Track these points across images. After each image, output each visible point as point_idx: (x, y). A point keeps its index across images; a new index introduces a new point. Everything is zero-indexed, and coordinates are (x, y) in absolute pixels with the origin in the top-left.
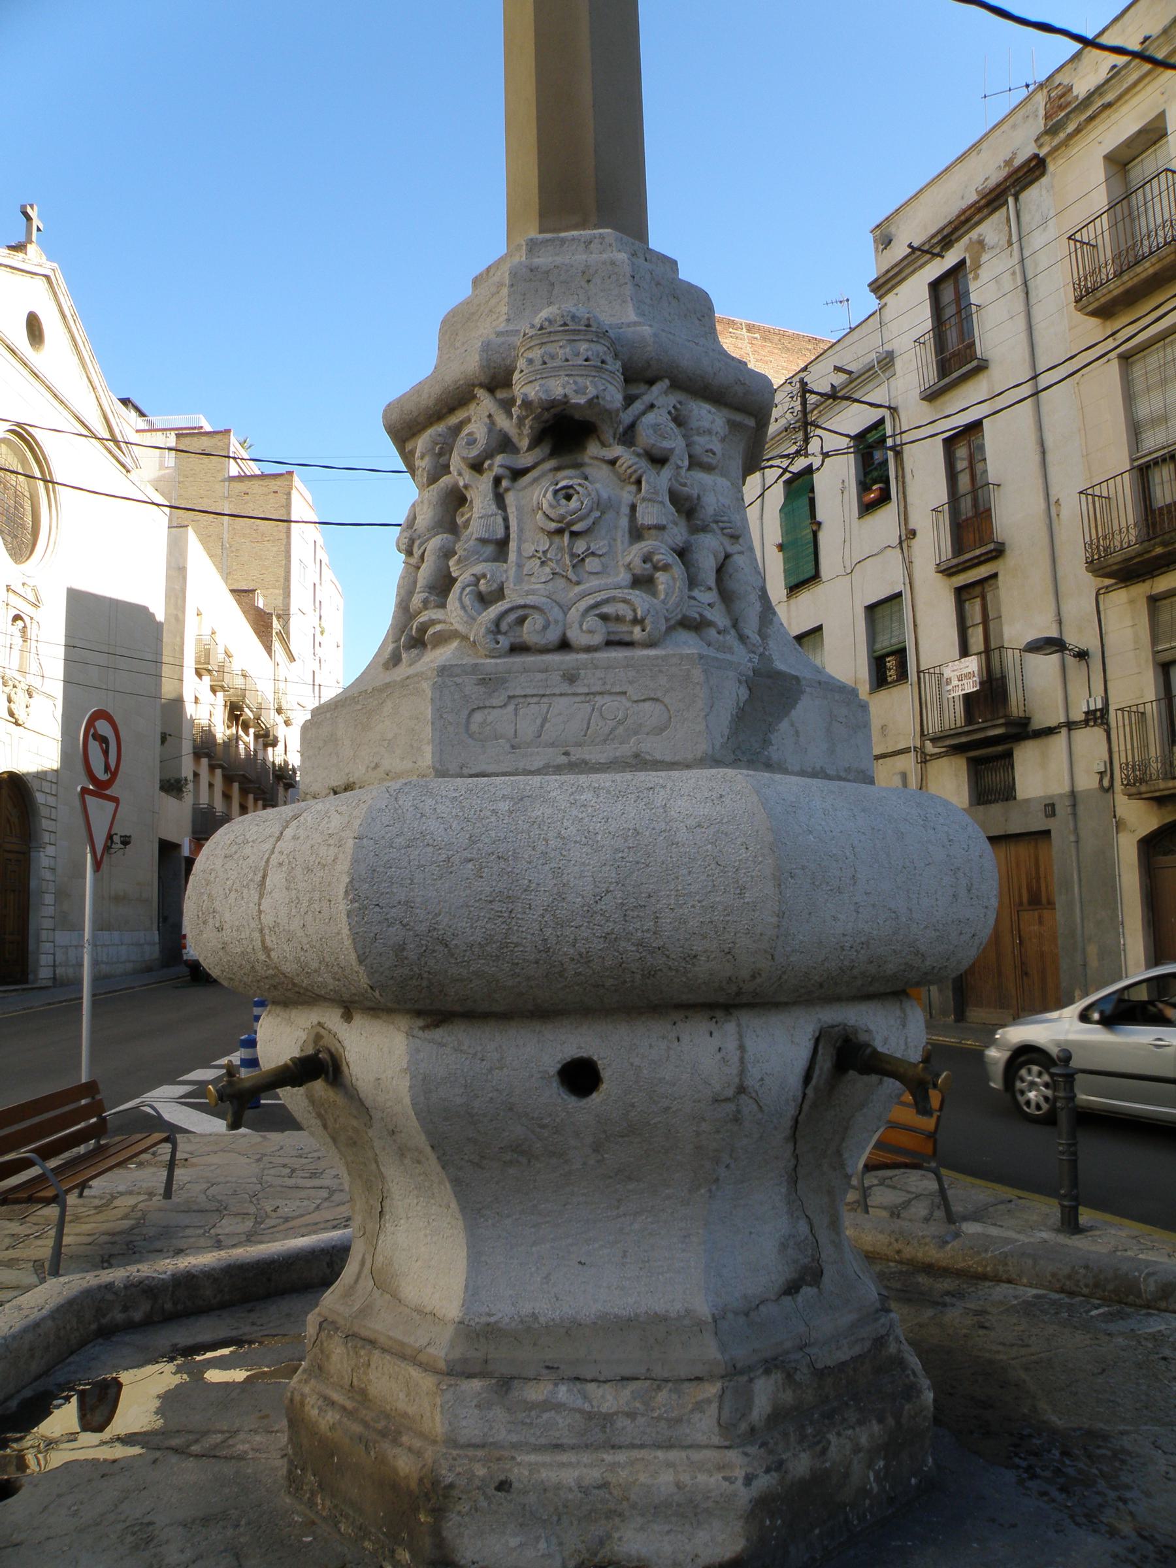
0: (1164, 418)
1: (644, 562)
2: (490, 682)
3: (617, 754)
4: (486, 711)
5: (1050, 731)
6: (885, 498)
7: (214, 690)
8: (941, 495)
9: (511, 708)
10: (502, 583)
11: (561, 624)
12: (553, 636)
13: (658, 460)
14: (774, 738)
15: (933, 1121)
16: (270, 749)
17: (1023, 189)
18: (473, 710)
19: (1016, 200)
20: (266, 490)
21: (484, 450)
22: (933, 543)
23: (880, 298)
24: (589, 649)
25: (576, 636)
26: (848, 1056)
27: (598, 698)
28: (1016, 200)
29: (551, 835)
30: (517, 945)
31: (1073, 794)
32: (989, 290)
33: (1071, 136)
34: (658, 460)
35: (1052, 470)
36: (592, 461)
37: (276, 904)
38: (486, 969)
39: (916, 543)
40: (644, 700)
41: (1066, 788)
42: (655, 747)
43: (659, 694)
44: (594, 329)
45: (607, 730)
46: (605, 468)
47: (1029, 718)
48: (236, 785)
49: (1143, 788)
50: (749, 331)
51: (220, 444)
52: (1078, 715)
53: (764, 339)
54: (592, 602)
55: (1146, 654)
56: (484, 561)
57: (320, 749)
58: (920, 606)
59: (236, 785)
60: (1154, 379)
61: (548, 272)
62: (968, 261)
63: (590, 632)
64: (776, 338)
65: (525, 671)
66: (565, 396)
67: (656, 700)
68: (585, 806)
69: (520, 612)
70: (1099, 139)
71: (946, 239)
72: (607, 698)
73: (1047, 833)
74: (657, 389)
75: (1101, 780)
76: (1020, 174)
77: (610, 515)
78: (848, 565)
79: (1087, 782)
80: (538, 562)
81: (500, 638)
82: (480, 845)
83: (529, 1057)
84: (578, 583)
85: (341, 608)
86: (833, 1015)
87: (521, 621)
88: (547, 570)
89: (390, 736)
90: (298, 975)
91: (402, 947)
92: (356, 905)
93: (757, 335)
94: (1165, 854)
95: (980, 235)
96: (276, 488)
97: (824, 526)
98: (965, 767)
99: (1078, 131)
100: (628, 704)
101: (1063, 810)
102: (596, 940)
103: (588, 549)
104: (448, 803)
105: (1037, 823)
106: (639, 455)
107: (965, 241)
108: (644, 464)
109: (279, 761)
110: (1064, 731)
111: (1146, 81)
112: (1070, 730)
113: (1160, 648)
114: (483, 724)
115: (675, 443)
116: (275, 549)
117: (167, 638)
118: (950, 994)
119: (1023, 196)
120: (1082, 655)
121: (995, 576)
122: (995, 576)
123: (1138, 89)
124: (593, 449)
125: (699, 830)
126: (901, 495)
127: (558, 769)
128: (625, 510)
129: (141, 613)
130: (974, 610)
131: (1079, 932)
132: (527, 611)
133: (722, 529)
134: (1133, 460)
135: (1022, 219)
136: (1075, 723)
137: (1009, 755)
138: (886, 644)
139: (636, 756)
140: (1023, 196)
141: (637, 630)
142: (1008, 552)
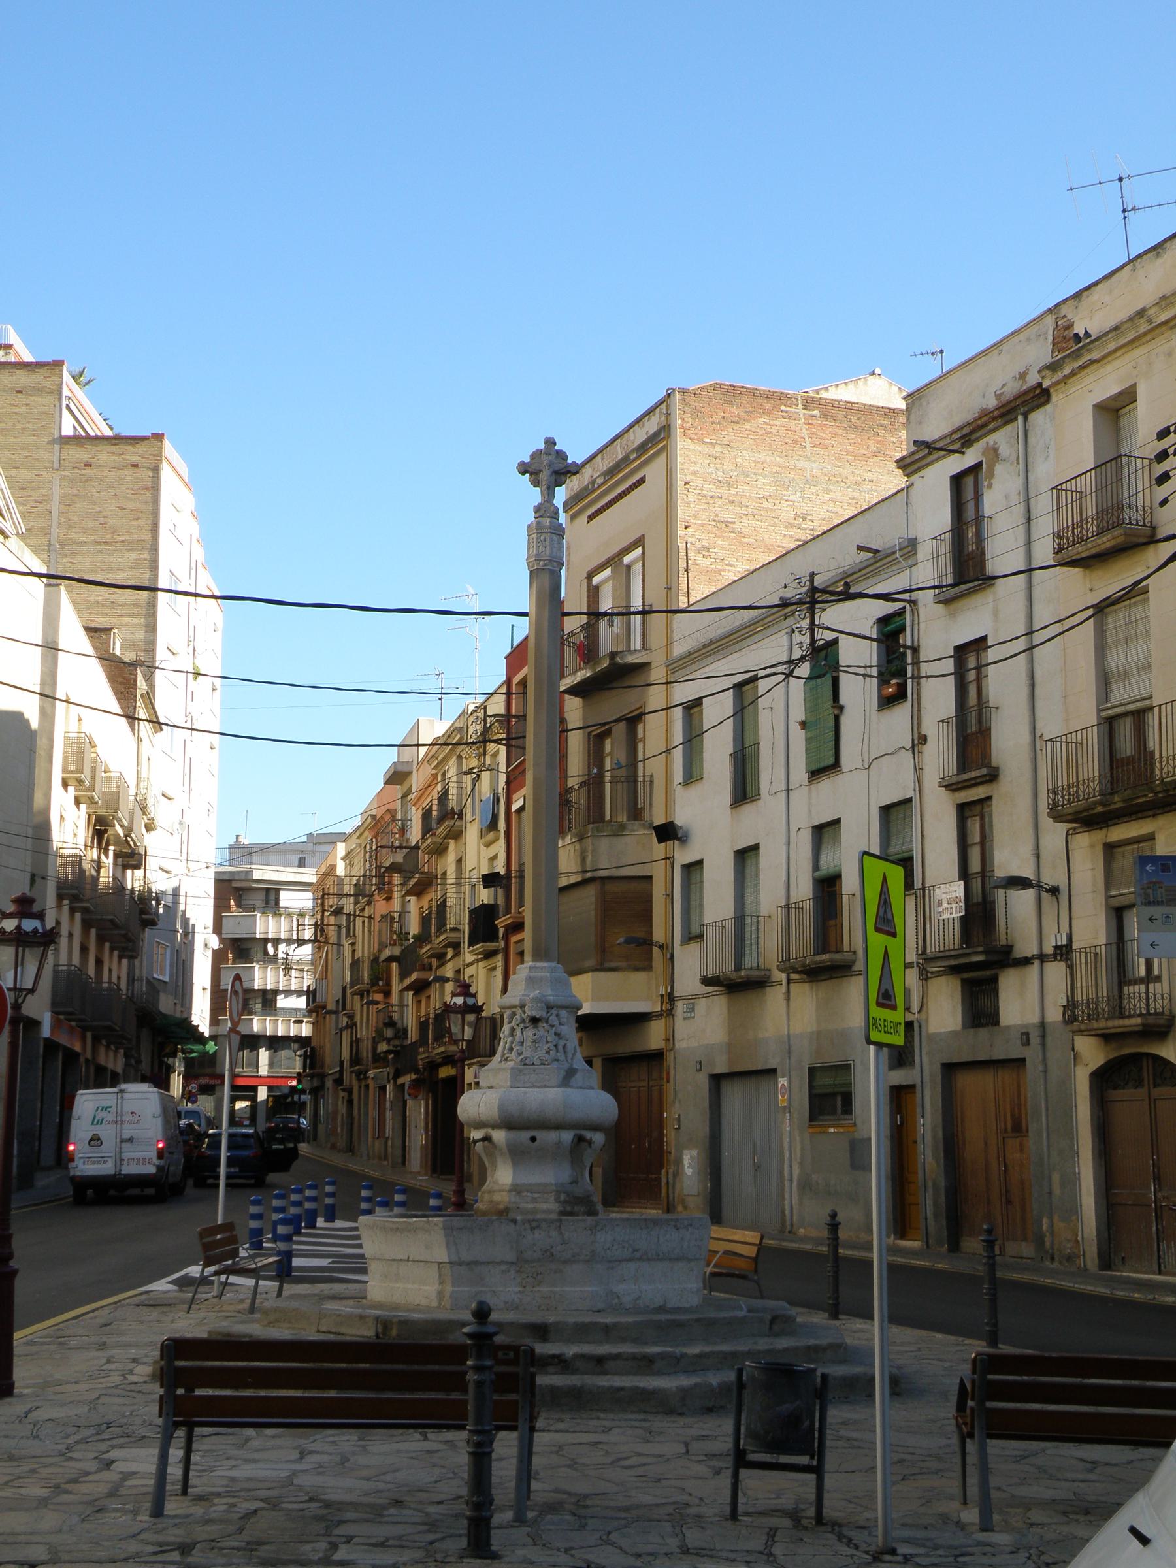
2: (520, 1071)
5: (1026, 961)
6: (900, 696)
7: (78, 802)
8: (948, 707)
13: (552, 1026)
16: (129, 872)
17: (1032, 410)
19: (1026, 419)
22: (940, 756)
23: (908, 475)
26: (580, 1139)
28: (1026, 419)
31: (1043, 1025)
32: (998, 498)
33: (1067, 377)
35: (1039, 704)
37: (482, 1109)
41: (1035, 1019)
47: (1012, 947)
48: (93, 932)
49: (1095, 1025)
50: (805, 407)
51: (46, 383)
52: (1048, 949)
53: (825, 416)
55: (1101, 898)
58: (927, 817)
59: (93, 932)
62: (984, 466)
64: (842, 413)
70: (1090, 387)
71: (966, 436)
73: (1023, 1060)
76: (1027, 398)
79: (1054, 1014)
83: (525, 1135)
85: (220, 626)
86: (578, 1132)
93: (816, 413)
94: (1115, 1089)
95: (995, 443)
96: (135, 459)
97: (846, 711)
98: (960, 988)
99: (1073, 374)
101: (1035, 1040)
105: (1014, 1051)
107: (983, 442)
109: (138, 886)
110: (1037, 963)
111: (1124, 350)
112: (1042, 962)
113: (1112, 893)
115: (556, 1023)
116: (134, 555)
117: (41, 743)
118: (944, 1222)
119: (1032, 416)
120: (1054, 891)
121: (990, 798)
122: (990, 798)
123: (1118, 354)
129: (16, 719)
130: (974, 827)
131: (1046, 1160)
134: (1100, 711)
135: (1030, 440)
137: (995, 980)
138: (898, 849)
140: (1033, 416)
142: (1001, 776)
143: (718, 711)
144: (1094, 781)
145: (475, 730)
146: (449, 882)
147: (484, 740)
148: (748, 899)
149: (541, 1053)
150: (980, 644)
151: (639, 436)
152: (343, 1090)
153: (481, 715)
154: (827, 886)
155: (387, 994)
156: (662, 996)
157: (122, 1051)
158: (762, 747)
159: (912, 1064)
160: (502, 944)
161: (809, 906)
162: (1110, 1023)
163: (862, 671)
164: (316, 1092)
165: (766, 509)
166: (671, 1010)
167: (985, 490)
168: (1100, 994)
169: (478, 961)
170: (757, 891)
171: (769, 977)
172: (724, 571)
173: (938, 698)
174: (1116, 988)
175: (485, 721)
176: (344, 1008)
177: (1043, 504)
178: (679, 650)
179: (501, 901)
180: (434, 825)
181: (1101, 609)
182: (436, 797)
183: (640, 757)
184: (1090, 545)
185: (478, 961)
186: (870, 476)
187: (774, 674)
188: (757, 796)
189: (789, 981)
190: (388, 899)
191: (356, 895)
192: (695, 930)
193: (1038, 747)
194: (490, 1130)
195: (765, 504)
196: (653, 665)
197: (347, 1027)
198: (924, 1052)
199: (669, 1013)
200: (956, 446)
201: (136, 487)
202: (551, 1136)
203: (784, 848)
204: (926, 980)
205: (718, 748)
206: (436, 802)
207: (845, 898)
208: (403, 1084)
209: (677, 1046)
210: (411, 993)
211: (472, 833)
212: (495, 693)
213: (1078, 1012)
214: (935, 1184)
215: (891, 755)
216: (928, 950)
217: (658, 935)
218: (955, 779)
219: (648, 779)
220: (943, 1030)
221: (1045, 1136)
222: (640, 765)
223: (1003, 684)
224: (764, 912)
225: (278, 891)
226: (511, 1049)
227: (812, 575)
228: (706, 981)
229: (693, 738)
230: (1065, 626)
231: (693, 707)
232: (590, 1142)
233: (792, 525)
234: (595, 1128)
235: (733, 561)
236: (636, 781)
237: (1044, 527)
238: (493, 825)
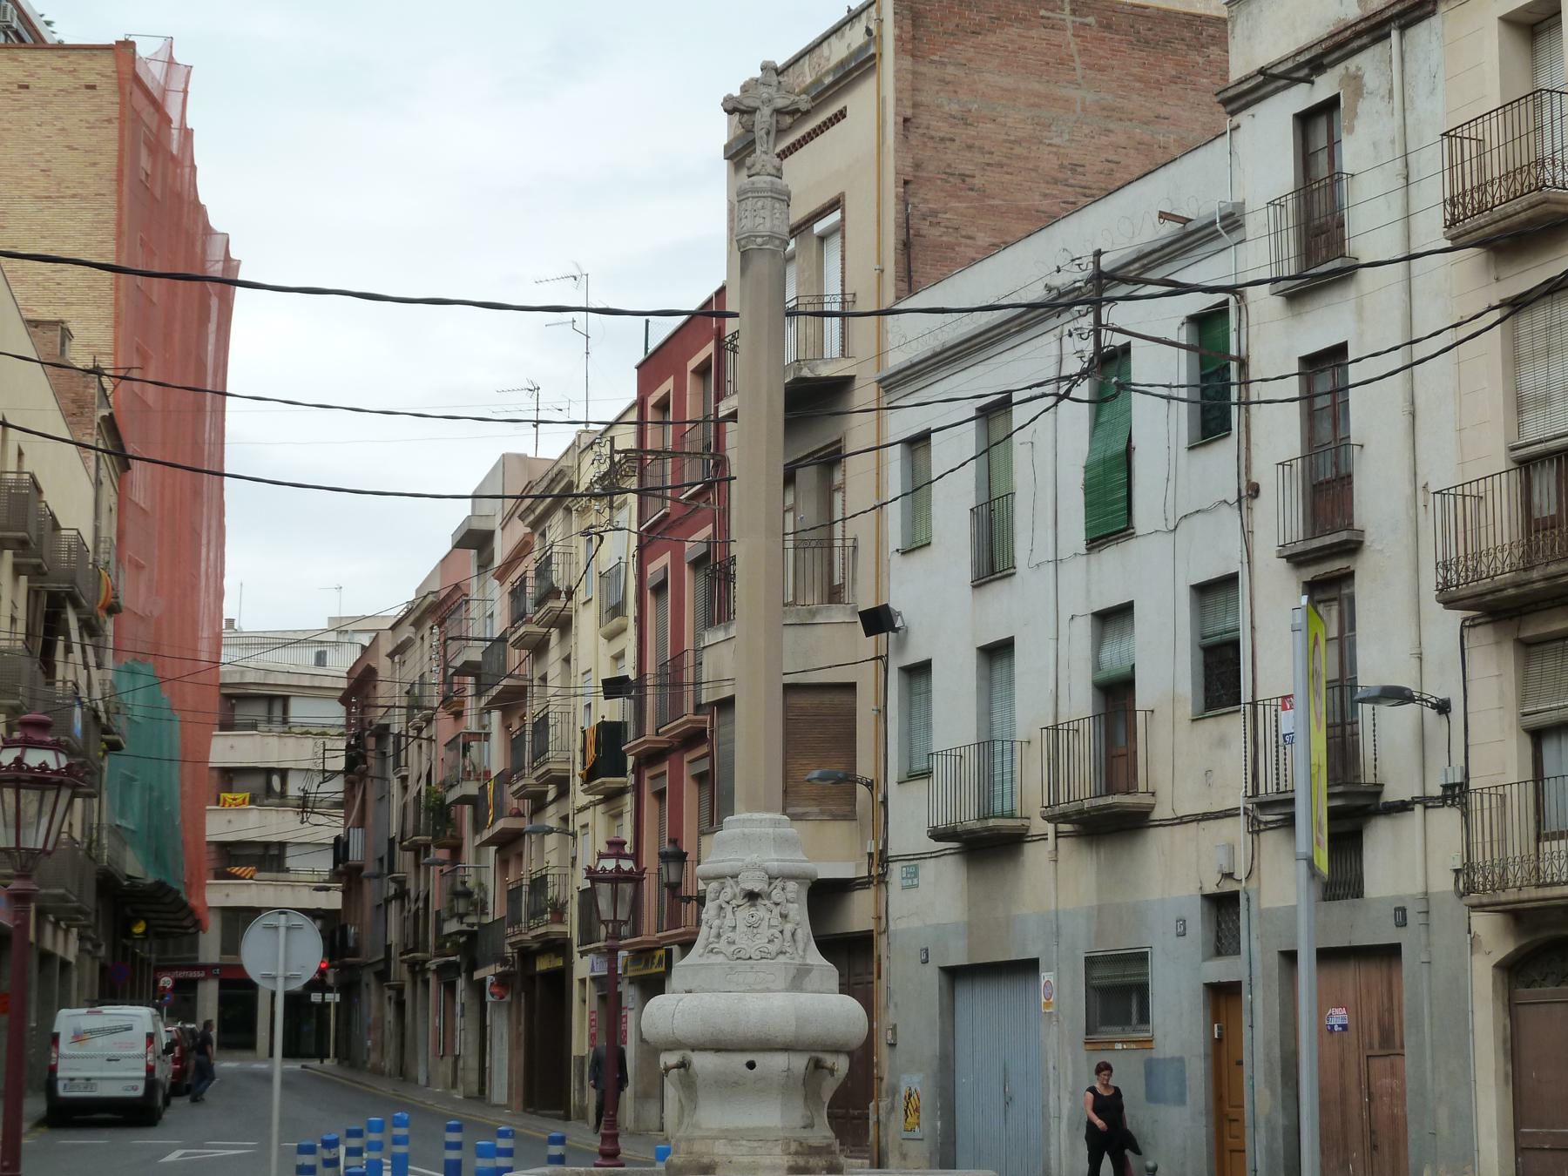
0: (1547, 400)
5: (1403, 807)
20: (66, 81)
22: (1280, 517)
26: (817, 1065)
32: (1361, 148)
34: (777, 904)
39: (1258, 504)
41: (1418, 889)
49: (1503, 897)
60: (1540, 344)
71: (1314, 63)
75: (1457, 881)
78: (1171, 517)
79: (1443, 883)
93: (1091, 20)
95: (1359, 69)
96: (91, 79)
105: (1384, 934)
107: (1340, 69)
110: (1418, 808)
112: (1426, 807)
120: (1443, 707)
124: (760, 901)
126: (1243, 428)
136: (1432, 798)
143: (955, 448)
144: (1502, 551)
145: (588, 473)
146: (551, 691)
147: (608, 488)
148: (997, 717)
149: (761, 941)
150: (1337, 353)
151: (838, 51)
152: (390, 987)
153: (606, 450)
154: (1116, 693)
155: (456, 851)
156: (870, 855)
157: (74, 931)
158: (1017, 498)
159: (1237, 952)
160: (630, 779)
161: (1087, 728)
162: (1524, 895)
163: (1165, 391)
164: (349, 989)
165: (1019, 157)
167: (1344, 137)
168: (1510, 854)
169: (595, 804)
170: (1011, 706)
171: (1028, 829)
172: (959, 245)
173: (1276, 432)
174: (1532, 844)
175: (612, 458)
176: (391, 870)
177: (1430, 161)
178: (896, 359)
179: (629, 718)
180: (530, 607)
181: (1516, 305)
182: (533, 566)
183: (838, 515)
184: (1497, 216)
185: (595, 804)
186: (1165, 111)
187: (1044, 395)
188: (1008, 573)
189: (1057, 835)
190: (458, 715)
191: (410, 708)
192: (919, 766)
193: (1420, 504)
194: (689, 1053)
195: (1018, 150)
196: (858, 383)
197: (396, 897)
198: (1253, 936)
199: (882, 880)
200: (1302, 74)
201: (92, 119)
202: (779, 1061)
203: (1052, 643)
204: (1258, 832)
205: (953, 503)
206: (531, 574)
207: (1140, 716)
208: (484, 980)
209: (892, 927)
210: (493, 849)
211: (587, 622)
212: (617, 422)
213: (1479, 879)
214: (1268, 1121)
215: (1208, 512)
216: (1262, 791)
217: (865, 766)
218: (1300, 548)
219: (849, 543)
220: (1281, 904)
222: (838, 527)
223: (1371, 414)
224: (1020, 735)
225: (285, 699)
226: (719, 936)
227: (1098, 254)
228: (937, 835)
229: (918, 488)
230: (1463, 332)
231: (918, 443)
232: (832, 1071)
233: (1056, 182)
234: (837, 1051)
235: (971, 231)
236: (831, 547)
237: (1432, 194)
238: (617, 610)
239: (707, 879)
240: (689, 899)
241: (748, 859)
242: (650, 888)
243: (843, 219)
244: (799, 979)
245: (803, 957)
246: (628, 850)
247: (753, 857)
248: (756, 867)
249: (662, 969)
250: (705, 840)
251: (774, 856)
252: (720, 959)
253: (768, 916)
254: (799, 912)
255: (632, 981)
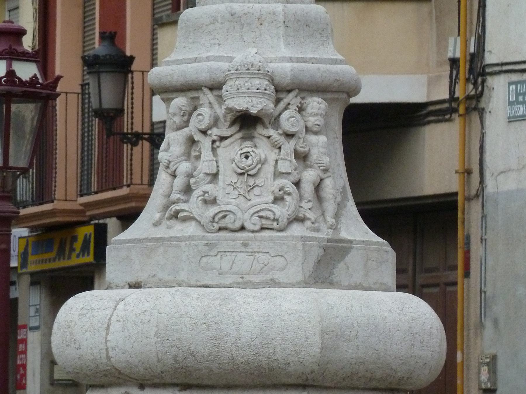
1: (280, 191)
3: (264, 279)
4: (208, 257)
9: (219, 257)
10: (216, 197)
11: (242, 220)
12: (238, 225)
14: (335, 271)
15: (108, 221)
18: (202, 257)
21: (208, 126)
24: (253, 232)
25: (247, 225)
27: (257, 254)
29: (235, 315)
30: (221, 356)
34: (289, 136)
36: (258, 136)
38: (208, 365)
40: (276, 256)
42: (279, 276)
43: (283, 254)
44: (262, 72)
45: (260, 268)
46: (265, 140)
54: (256, 210)
56: (208, 183)
57: (120, 262)
61: (240, 17)
63: (254, 224)
65: (226, 240)
66: (247, 108)
67: (282, 256)
68: (249, 304)
69: (224, 213)
72: (261, 254)
74: (291, 95)
77: (266, 167)
80: (233, 187)
81: (215, 224)
82: (208, 318)
84: (250, 200)
87: (224, 217)
88: (236, 192)
89: (162, 263)
90: (124, 368)
91: (176, 356)
92: (159, 339)
100: (270, 257)
102: (251, 356)
103: (255, 183)
104: (195, 300)
106: (281, 135)
108: (282, 139)
114: (207, 263)
124: (260, 130)
125: (292, 315)
127: (239, 286)
128: (272, 163)
132: (227, 213)
133: (320, 167)
139: (272, 280)
141: (275, 223)
149: (262, 199)
156: (454, 62)
166: (479, 96)
221: (34, 179)
226: (188, 190)
239: (168, 91)
240: (136, 138)
241: (239, 57)
242: (67, 115)
243: (206, 87)
244: (326, 266)
245: (334, 228)
246: (28, 43)
247: (246, 54)
248: (251, 71)
249: (90, 259)
250: (164, 35)
251: (285, 52)
252: (190, 229)
253: (272, 156)
254: (327, 149)
255: (36, 279)
